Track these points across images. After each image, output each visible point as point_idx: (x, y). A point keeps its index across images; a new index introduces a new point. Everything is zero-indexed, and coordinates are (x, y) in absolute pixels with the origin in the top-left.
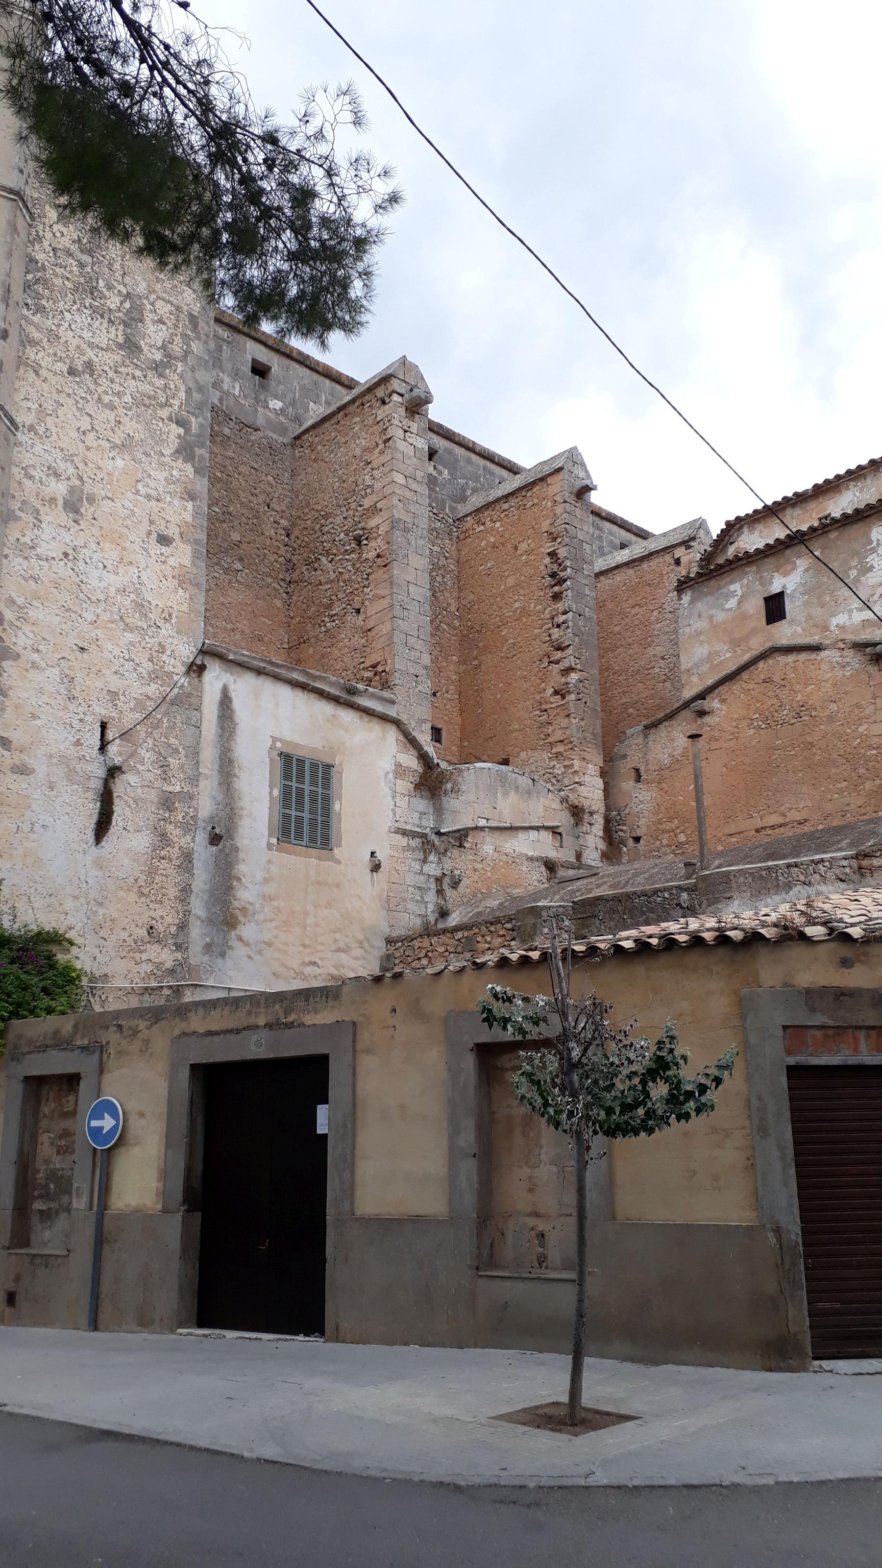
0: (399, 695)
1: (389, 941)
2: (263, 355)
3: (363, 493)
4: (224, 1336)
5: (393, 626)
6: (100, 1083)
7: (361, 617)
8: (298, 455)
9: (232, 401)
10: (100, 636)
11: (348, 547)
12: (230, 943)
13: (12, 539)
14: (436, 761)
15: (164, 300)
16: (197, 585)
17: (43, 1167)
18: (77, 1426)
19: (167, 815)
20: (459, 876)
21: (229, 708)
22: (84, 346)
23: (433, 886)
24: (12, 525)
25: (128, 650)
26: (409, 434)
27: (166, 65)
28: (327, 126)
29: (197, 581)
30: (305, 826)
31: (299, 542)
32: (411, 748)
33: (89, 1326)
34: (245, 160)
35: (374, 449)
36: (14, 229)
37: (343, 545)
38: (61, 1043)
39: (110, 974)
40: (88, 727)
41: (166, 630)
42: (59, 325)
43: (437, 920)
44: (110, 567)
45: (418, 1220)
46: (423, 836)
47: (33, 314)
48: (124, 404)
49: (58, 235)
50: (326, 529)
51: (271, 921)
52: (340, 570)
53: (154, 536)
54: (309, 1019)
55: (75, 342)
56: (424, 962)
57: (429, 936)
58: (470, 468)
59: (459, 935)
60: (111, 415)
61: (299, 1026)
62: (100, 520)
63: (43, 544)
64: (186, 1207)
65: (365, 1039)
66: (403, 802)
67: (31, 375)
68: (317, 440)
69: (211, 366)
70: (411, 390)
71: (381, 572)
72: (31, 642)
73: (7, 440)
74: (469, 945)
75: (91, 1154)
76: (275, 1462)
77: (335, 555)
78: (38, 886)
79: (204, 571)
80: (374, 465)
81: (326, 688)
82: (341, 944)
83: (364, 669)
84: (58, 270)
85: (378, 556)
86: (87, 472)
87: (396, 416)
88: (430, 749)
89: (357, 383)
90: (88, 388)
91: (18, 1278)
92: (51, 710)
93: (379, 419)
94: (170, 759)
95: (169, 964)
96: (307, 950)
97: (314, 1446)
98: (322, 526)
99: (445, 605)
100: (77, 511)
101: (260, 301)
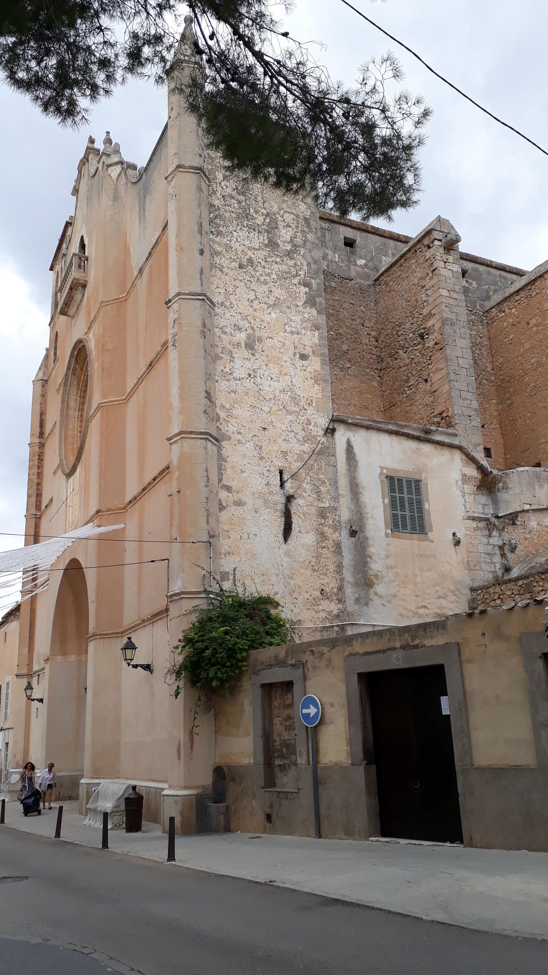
0: (459, 430)
1: (473, 590)
2: (350, 233)
3: (422, 306)
4: (399, 843)
5: (450, 387)
6: (305, 686)
7: (429, 384)
8: (378, 290)
9: (334, 265)
10: (274, 420)
11: (416, 342)
12: (370, 597)
13: (219, 371)
14: (489, 470)
15: (288, 212)
16: (325, 381)
17: (278, 739)
18: (318, 895)
19: (323, 521)
20: (515, 544)
21: (352, 452)
22: (246, 250)
23: (498, 552)
24: (218, 362)
25: (290, 425)
26: (447, 264)
27: (279, 73)
28: (378, 83)
29: (325, 378)
30: (408, 520)
31: (384, 344)
32: (472, 463)
33: (316, 834)
34: (331, 117)
35: (426, 277)
36: (200, 189)
37: (412, 341)
38: (280, 663)
39: (302, 620)
40: (273, 474)
41: (310, 411)
42: (231, 240)
43: (503, 574)
44: (275, 379)
45: (516, 769)
46: (487, 520)
47: (216, 237)
48: (272, 280)
49: (224, 187)
50: (400, 333)
51: (394, 581)
52: (412, 357)
53: (298, 355)
54: (428, 642)
55: (241, 248)
56: (498, 602)
57: (499, 585)
58: (490, 277)
59: (520, 583)
60: (265, 288)
61: (422, 647)
62: (266, 351)
63: (236, 370)
64: (366, 762)
65: (466, 653)
66: (470, 499)
67: (219, 273)
68: (389, 279)
69: (320, 246)
70: (446, 236)
71: (439, 353)
72: (235, 429)
73: (210, 313)
74: (528, 589)
75: (304, 730)
76: (444, 924)
77: (408, 348)
78: (256, 570)
79: (329, 372)
80: (427, 287)
81: (411, 432)
82: (441, 594)
83: (434, 416)
84: (227, 208)
85: (436, 344)
86: (257, 323)
87: (438, 254)
88: (484, 462)
89: (411, 238)
90: (251, 274)
91: (271, 806)
92: (251, 467)
93: (427, 258)
94: (321, 487)
95: (335, 612)
96: (419, 599)
97: (467, 914)
98: (398, 331)
99: (484, 368)
100: (252, 348)
101: (344, 201)
